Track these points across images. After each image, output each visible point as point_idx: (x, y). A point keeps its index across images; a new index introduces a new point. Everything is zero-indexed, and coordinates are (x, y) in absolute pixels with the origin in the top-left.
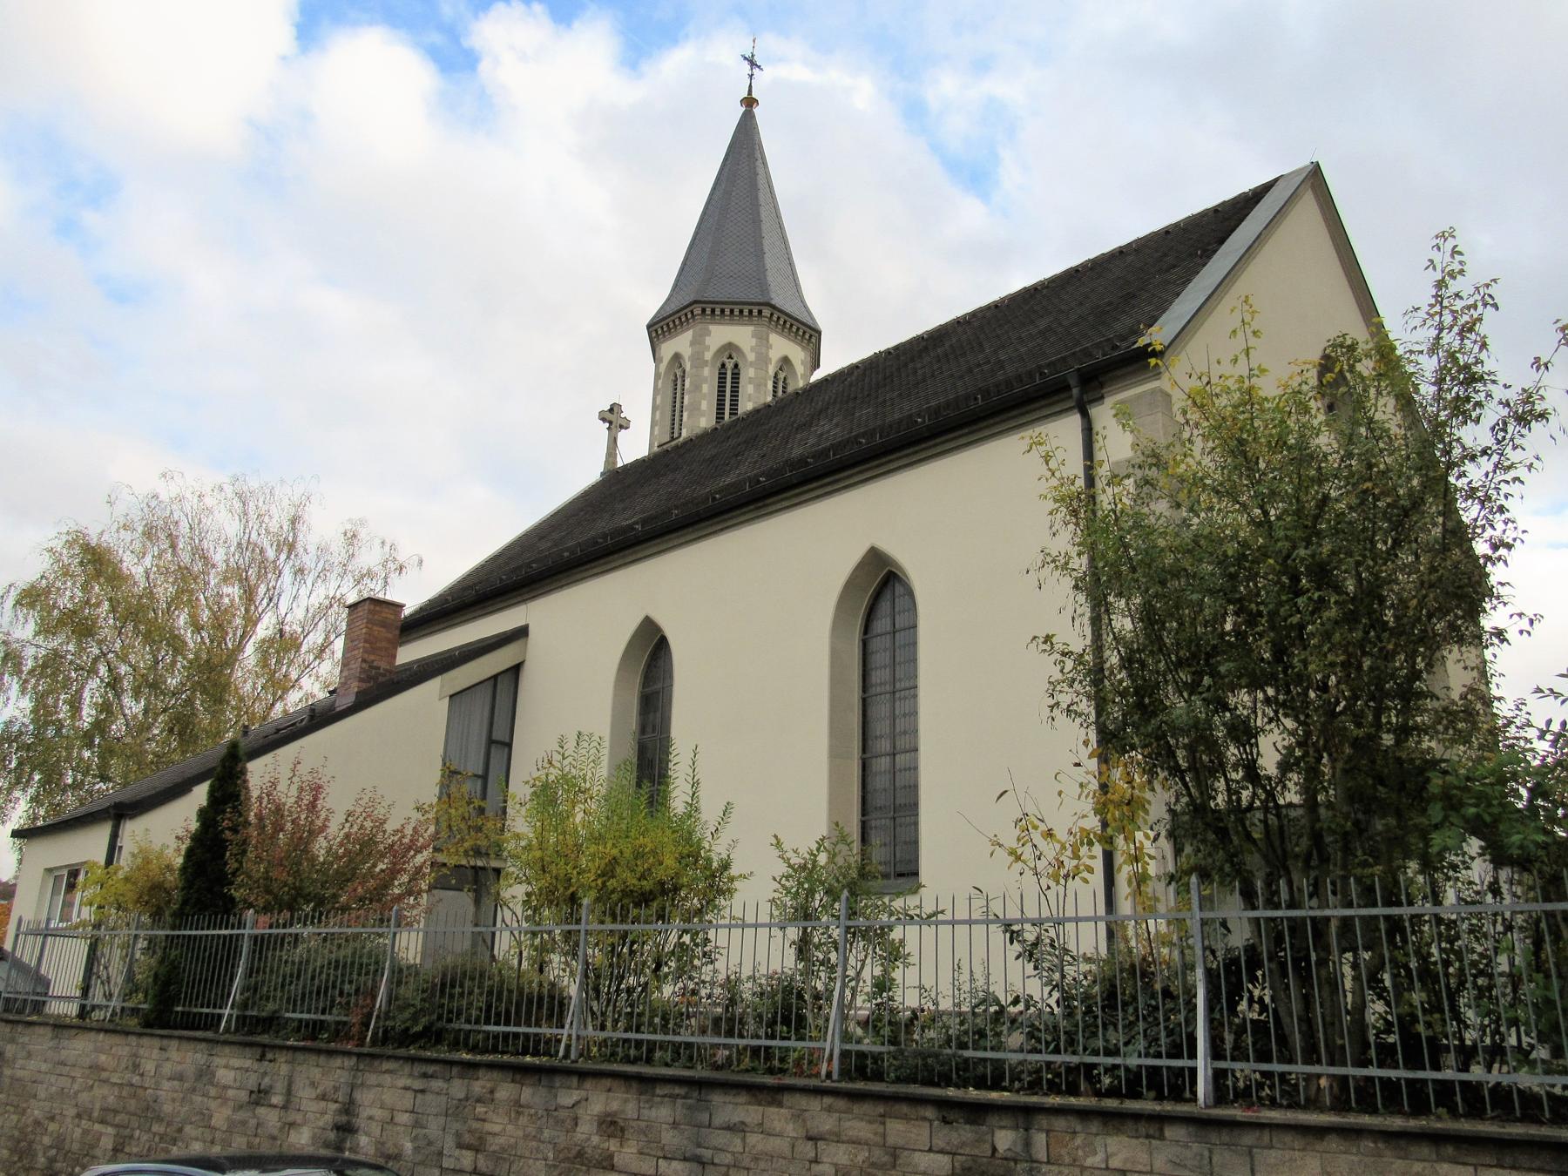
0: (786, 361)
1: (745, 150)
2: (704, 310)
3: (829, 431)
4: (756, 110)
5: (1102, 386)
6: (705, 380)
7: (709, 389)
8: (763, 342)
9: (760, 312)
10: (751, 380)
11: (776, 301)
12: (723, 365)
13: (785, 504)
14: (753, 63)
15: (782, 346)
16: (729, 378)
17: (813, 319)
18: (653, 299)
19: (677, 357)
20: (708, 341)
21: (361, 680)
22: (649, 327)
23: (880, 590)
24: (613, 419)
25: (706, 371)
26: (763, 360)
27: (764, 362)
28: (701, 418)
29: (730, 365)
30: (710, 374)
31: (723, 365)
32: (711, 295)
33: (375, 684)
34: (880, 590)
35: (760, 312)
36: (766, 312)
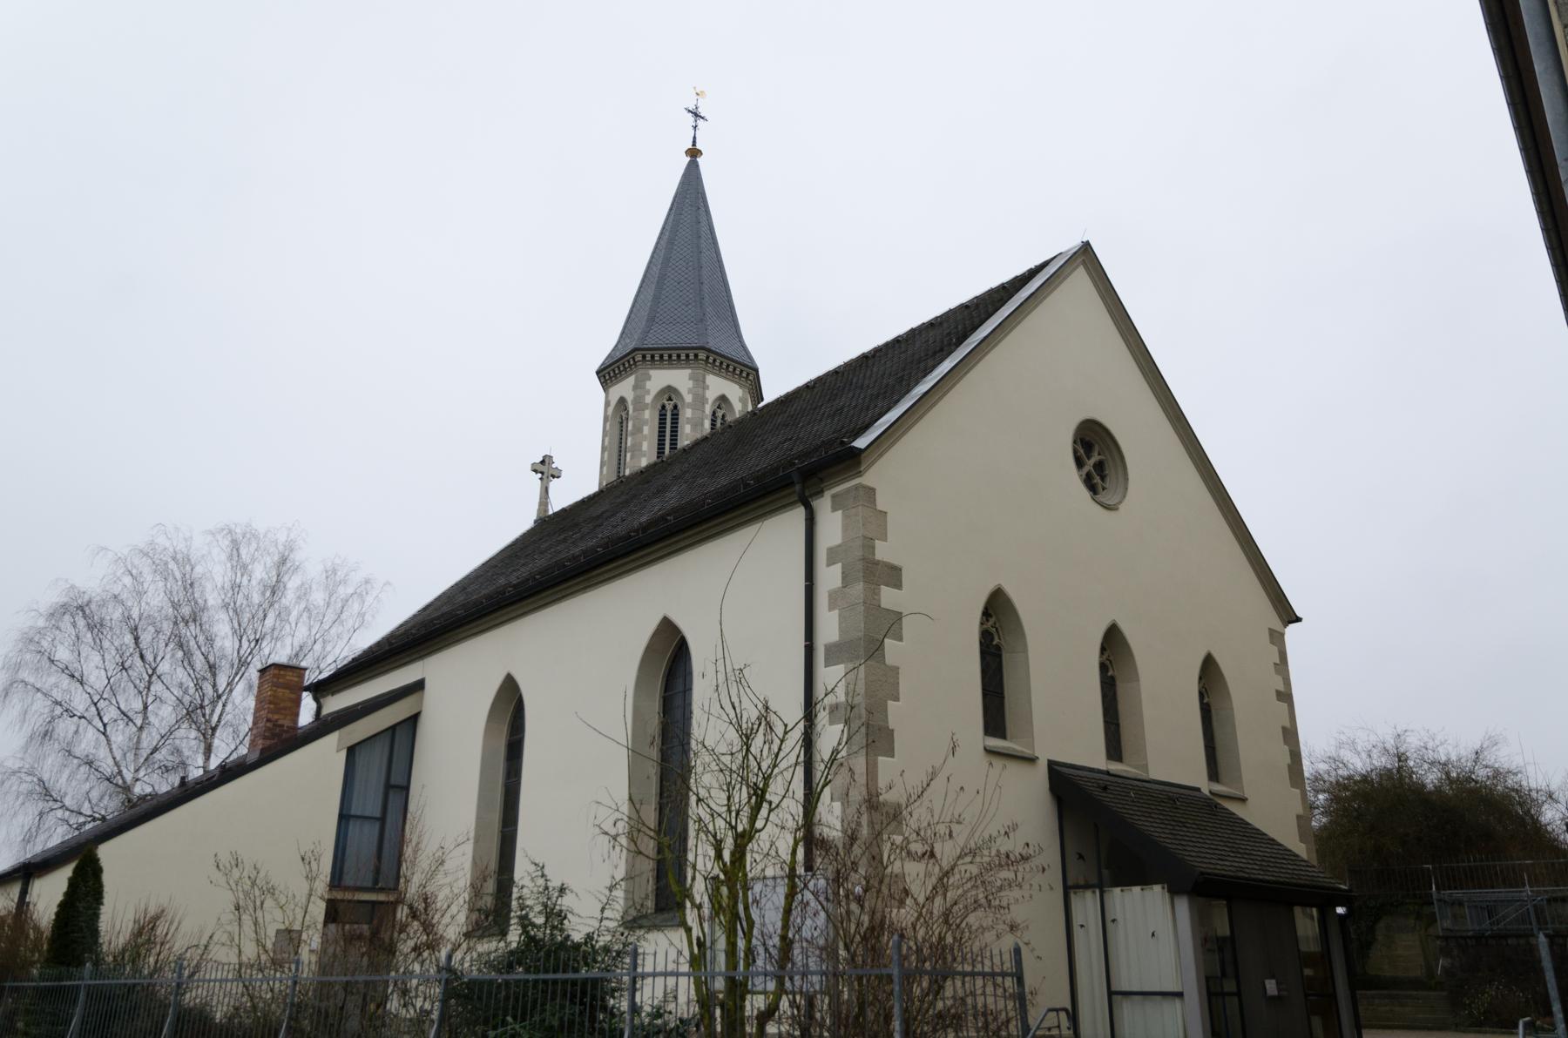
0: (723, 399)
1: (690, 202)
3: (756, 461)
5: (822, 480)
6: (646, 422)
7: (649, 431)
8: (701, 384)
10: (688, 421)
11: (712, 345)
12: (663, 407)
13: (688, 542)
14: (696, 115)
15: (718, 385)
16: (669, 417)
17: (750, 358)
18: (604, 340)
19: (622, 401)
20: (649, 385)
21: (265, 738)
22: (598, 373)
23: (670, 658)
24: (546, 469)
25: (647, 414)
26: (700, 400)
27: (705, 397)
28: (644, 455)
29: (669, 407)
30: (650, 416)
31: (663, 407)
33: (277, 739)
34: (670, 658)
36: (702, 355)
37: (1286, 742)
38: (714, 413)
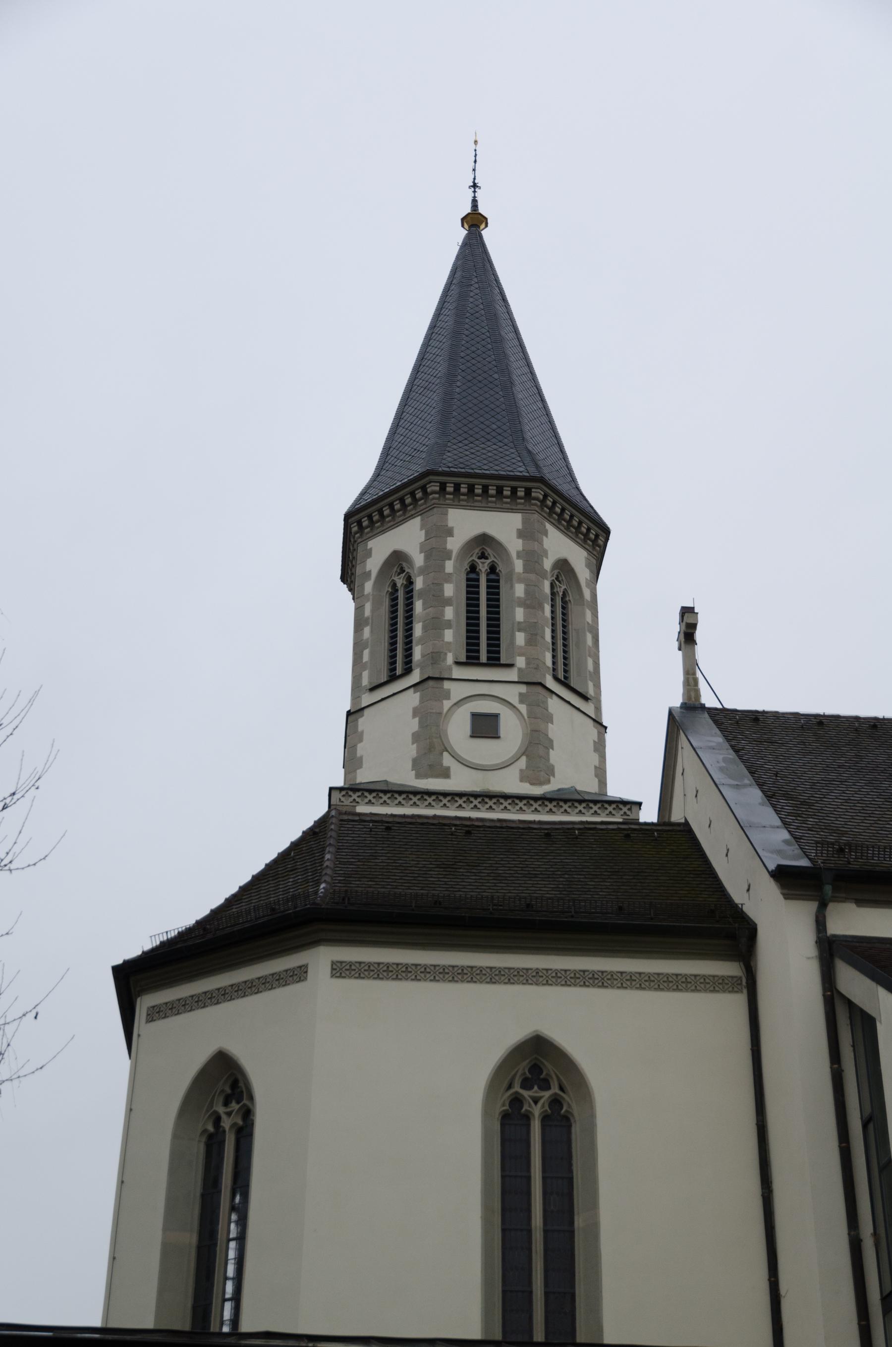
2: (443, 486)
4: (486, 233)
8: (438, 533)
9: (528, 492)
12: (473, 568)
18: (355, 469)
22: (348, 517)
26: (532, 558)
29: (483, 567)
31: (473, 568)
32: (448, 462)
35: (528, 492)
36: (538, 494)
37: (596, 776)
38: (553, 594)
